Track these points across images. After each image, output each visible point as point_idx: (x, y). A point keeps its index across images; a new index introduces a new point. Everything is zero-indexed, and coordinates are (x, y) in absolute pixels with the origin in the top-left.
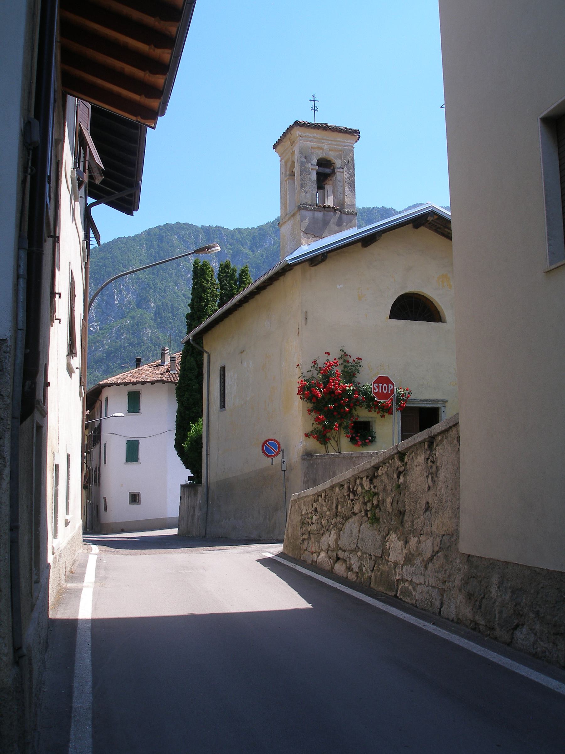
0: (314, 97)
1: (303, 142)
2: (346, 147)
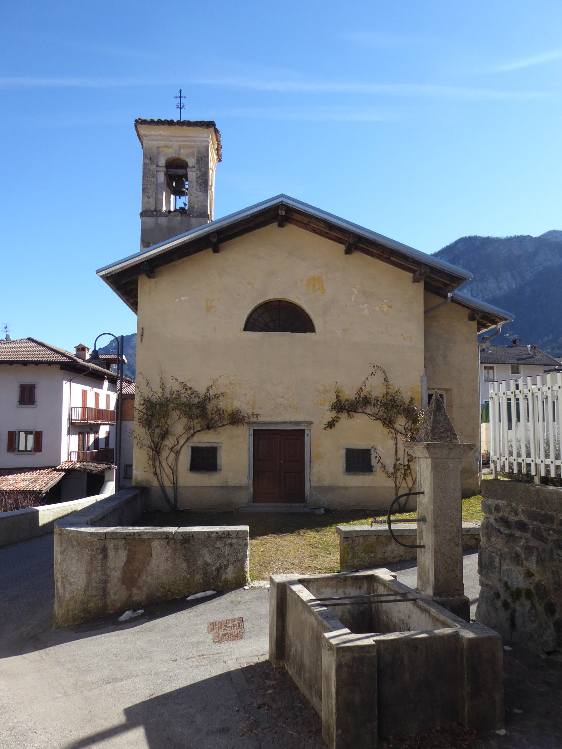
0: (180, 93)
1: (148, 142)
2: (199, 143)
